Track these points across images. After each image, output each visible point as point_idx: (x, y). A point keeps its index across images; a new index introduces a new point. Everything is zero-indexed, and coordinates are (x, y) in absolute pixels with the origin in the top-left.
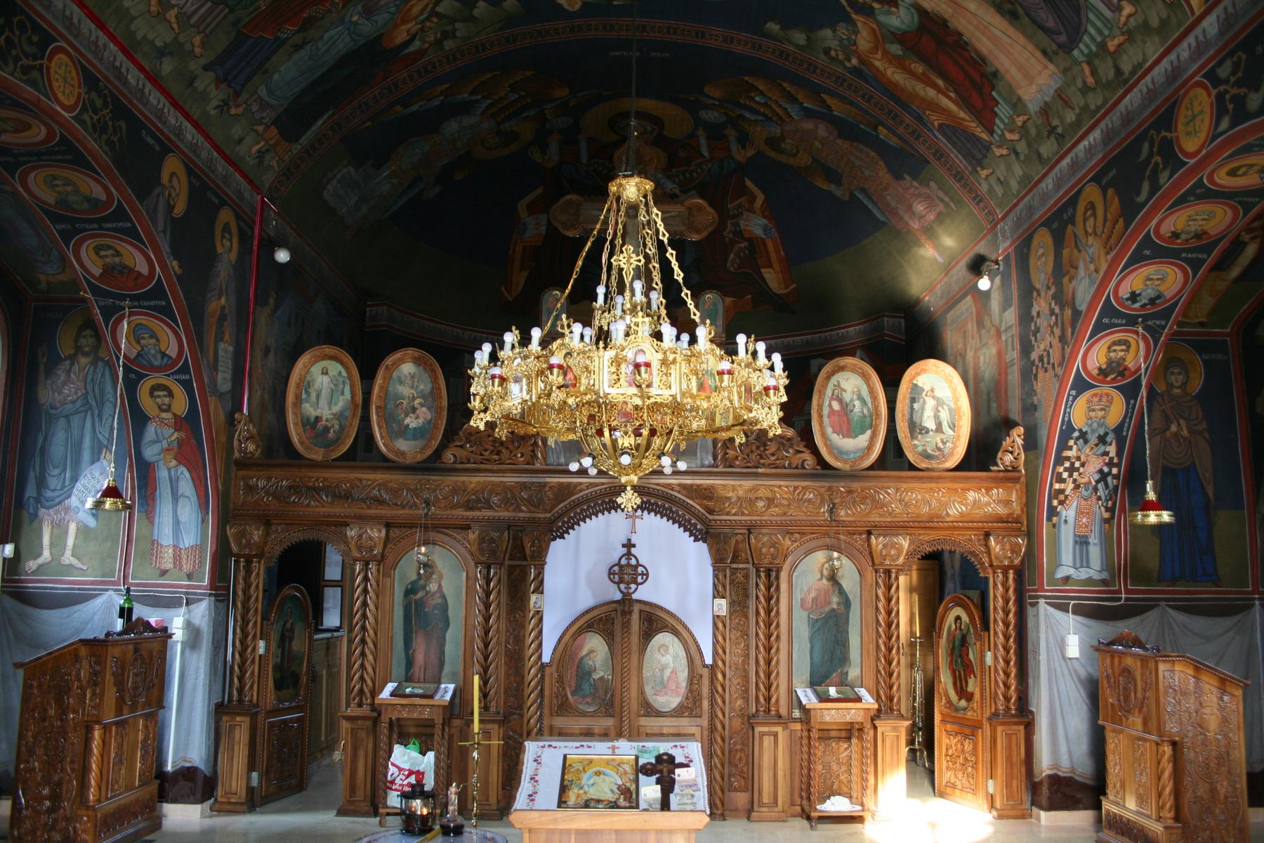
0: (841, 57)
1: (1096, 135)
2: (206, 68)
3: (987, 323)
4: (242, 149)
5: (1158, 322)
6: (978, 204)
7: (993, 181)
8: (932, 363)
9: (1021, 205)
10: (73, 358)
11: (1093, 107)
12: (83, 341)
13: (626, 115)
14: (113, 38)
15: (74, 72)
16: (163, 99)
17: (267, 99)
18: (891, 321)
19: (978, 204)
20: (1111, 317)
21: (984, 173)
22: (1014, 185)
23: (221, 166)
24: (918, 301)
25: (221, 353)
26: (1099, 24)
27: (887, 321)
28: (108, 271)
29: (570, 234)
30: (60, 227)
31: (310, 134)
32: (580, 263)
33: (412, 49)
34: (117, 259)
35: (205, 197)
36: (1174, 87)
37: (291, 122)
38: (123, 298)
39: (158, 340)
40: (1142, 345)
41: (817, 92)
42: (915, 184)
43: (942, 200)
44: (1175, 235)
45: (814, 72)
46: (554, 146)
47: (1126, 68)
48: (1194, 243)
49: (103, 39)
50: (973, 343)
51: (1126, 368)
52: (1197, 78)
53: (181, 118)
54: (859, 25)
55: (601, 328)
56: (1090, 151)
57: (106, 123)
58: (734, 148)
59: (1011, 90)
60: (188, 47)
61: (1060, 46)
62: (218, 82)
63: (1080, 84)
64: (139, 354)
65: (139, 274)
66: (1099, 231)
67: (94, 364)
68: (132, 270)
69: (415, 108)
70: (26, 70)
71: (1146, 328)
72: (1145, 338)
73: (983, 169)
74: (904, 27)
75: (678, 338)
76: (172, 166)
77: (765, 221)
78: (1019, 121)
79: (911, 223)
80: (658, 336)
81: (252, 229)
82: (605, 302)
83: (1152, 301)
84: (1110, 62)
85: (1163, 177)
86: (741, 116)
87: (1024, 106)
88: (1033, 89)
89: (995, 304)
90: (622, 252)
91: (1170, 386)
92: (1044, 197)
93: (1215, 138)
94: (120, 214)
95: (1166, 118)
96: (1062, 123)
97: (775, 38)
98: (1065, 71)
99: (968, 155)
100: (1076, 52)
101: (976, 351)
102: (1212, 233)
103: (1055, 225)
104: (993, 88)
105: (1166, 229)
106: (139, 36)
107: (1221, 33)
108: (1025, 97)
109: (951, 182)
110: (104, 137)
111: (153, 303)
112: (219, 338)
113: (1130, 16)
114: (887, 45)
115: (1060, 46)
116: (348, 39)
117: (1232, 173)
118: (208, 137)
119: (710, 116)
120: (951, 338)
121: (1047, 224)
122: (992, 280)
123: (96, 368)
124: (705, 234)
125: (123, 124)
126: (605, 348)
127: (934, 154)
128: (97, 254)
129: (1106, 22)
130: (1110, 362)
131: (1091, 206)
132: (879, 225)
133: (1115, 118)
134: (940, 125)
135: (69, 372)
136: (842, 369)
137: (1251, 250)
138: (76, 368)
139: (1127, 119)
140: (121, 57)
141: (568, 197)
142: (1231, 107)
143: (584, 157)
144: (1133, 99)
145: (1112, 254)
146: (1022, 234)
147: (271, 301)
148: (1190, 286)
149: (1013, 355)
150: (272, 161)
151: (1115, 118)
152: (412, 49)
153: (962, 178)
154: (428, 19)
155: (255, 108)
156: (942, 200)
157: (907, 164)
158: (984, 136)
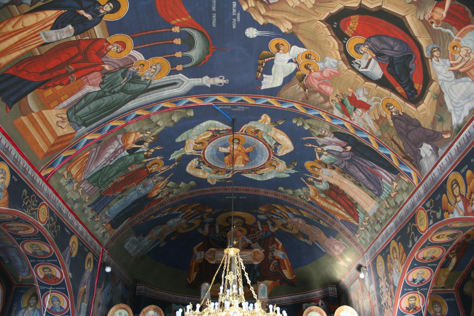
0: (305, 198)
1: (392, 224)
2: (89, 206)
3: (365, 290)
4: (97, 232)
5: (425, 289)
6: (357, 246)
7: (361, 238)
8: (345, 307)
9: (371, 247)
10: (26, 308)
11: (390, 214)
12: (31, 301)
13: (231, 217)
14: (60, 198)
15: (46, 211)
16: (73, 217)
17: (108, 215)
18: (331, 288)
19: (357, 246)
20: (407, 288)
21: (357, 236)
22: (368, 240)
23: (90, 238)
24: (340, 281)
25: (82, 306)
26: (387, 188)
27: (330, 289)
28: (46, 277)
29: (212, 262)
30: (31, 261)
31: (121, 226)
32: (214, 278)
33: (158, 197)
34: (50, 273)
35: (83, 249)
36: (414, 209)
37: (115, 223)
38: (50, 286)
39: (60, 302)
40: (420, 298)
41: (298, 209)
42: (334, 239)
43: (344, 245)
44: (424, 258)
45: (296, 203)
46: (207, 228)
47: (398, 202)
48: (431, 261)
49: (57, 199)
50: (361, 297)
51: (416, 307)
52: (420, 207)
53: (79, 223)
54: (310, 188)
55: (221, 302)
56: (391, 229)
57: (54, 227)
58: (270, 227)
59: (362, 209)
60: (84, 200)
61: (376, 195)
62: (92, 210)
63: (385, 207)
64: (52, 307)
65: (57, 278)
66: (398, 257)
67: (34, 310)
68: (54, 276)
69: (158, 216)
70: (32, 212)
71: (421, 291)
72: (421, 295)
73: (357, 234)
74: (325, 189)
75: (249, 305)
76: (74, 239)
77: (283, 253)
78: (367, 218)
79: (335, 253)
80: (240, 305)
81: (98, 260)
82: (223, 293)
83: (421, 282)
84: (393, 200)
85: (416, 239)
86: (272, 217)
87: (368, 214)
88: (370, 208)
89: (367, 282)
90: (229, 274)
91: (436, 312)
92: (379, 245)
93: (429, 227)
94: (54, 257)
95: (413, 219)
96: (381, 219)
97: (282, 192)
98: (379, 203)
99: (351, 230)
100: (381, 197)
101: (362, 300)
102: (437, 257)
103: (383, 255)
104: (357, 208)
105: (420, 256)
106: (69, 197)
107: (425, 193)
108: (368, 211)
109: (346, 238)
110: (53, 231)
111: (60, 288)
112: (82, 301)
113: (396, 186)
114: (320, 194)
115: (376, 195)
116: (137, 195)
117: (438, 237)
118: (87, 229)
119: (262, 217)
120: (353, 296)
121: (381, 254)
122: (365, 274)
123: (34, 312)
124: (260, 262)
125: (59, 226)
126: (222, 311)
127: (340, 230)
128: (43, 270)
129: (389, 188)
130: (410, 305)
131: (394, 248)
132: (324, 254)
133: (397, 218)
134: (341, 220)
135: (24, 313)
136: (312, 310)
137: (454, 260)
138: (27, 312)
139: (401, 219)
140: (62, 204)
141: (211, 249)
142: (432, 216)
143: (217, 231)
144: (402, 212)
145: (404, 266)
146: (373, 257)
147: (103, 286)
148: (433, 276)
149: (375, 302)
150: (107, 235)
151: (397, 218)
152: (158, 197)
153: (350, 237)
154: (164, 188)
155: (104, 218)
156: (344, 245)
157: (330, 232)
158: (356, 223)
